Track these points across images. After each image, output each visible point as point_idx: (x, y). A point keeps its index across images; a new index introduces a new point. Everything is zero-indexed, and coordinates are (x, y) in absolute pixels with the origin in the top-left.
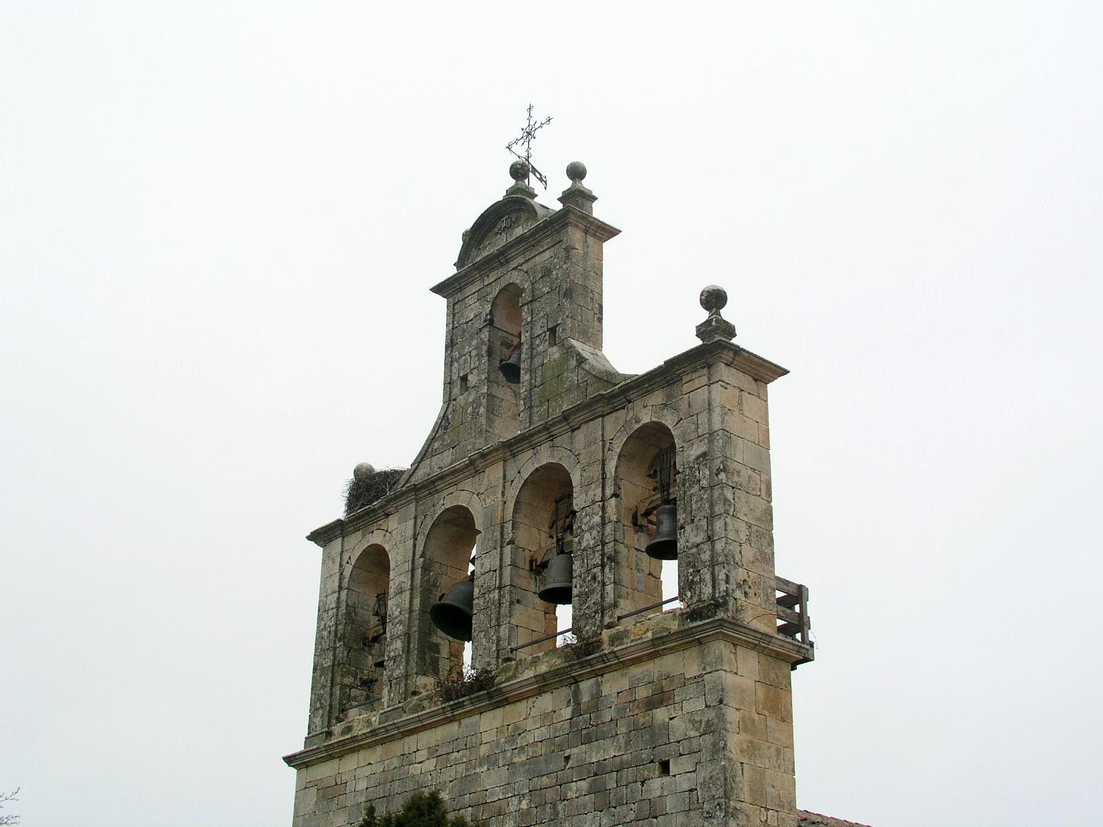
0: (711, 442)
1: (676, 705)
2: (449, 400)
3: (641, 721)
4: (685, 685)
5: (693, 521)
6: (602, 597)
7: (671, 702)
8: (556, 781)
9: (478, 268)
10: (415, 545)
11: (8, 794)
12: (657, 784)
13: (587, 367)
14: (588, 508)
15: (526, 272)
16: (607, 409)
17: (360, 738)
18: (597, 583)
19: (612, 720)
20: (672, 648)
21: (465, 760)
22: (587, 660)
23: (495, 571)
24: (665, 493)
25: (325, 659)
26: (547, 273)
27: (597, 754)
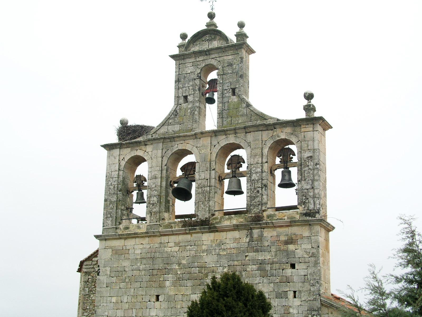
0: (314, 152)
1: (299, 245)
2: (178, 104)
3: (282, 248)
4: (302, 239)
5: (305, 180)
7: (296, 243)
8: (241, 263)
9: (195, 53)
11: (357, 297)
12: (289, 271)
13: (252, 109)
14: (254, 165)
16: (264, 129)
17: (139, 234)
19: (268, 246)
20: (297, 225)
21: (195, 250)
22: (260, 223)
24: (286, 164)
25: (112, 198)
26: (230, 65)
27: (261, 257)
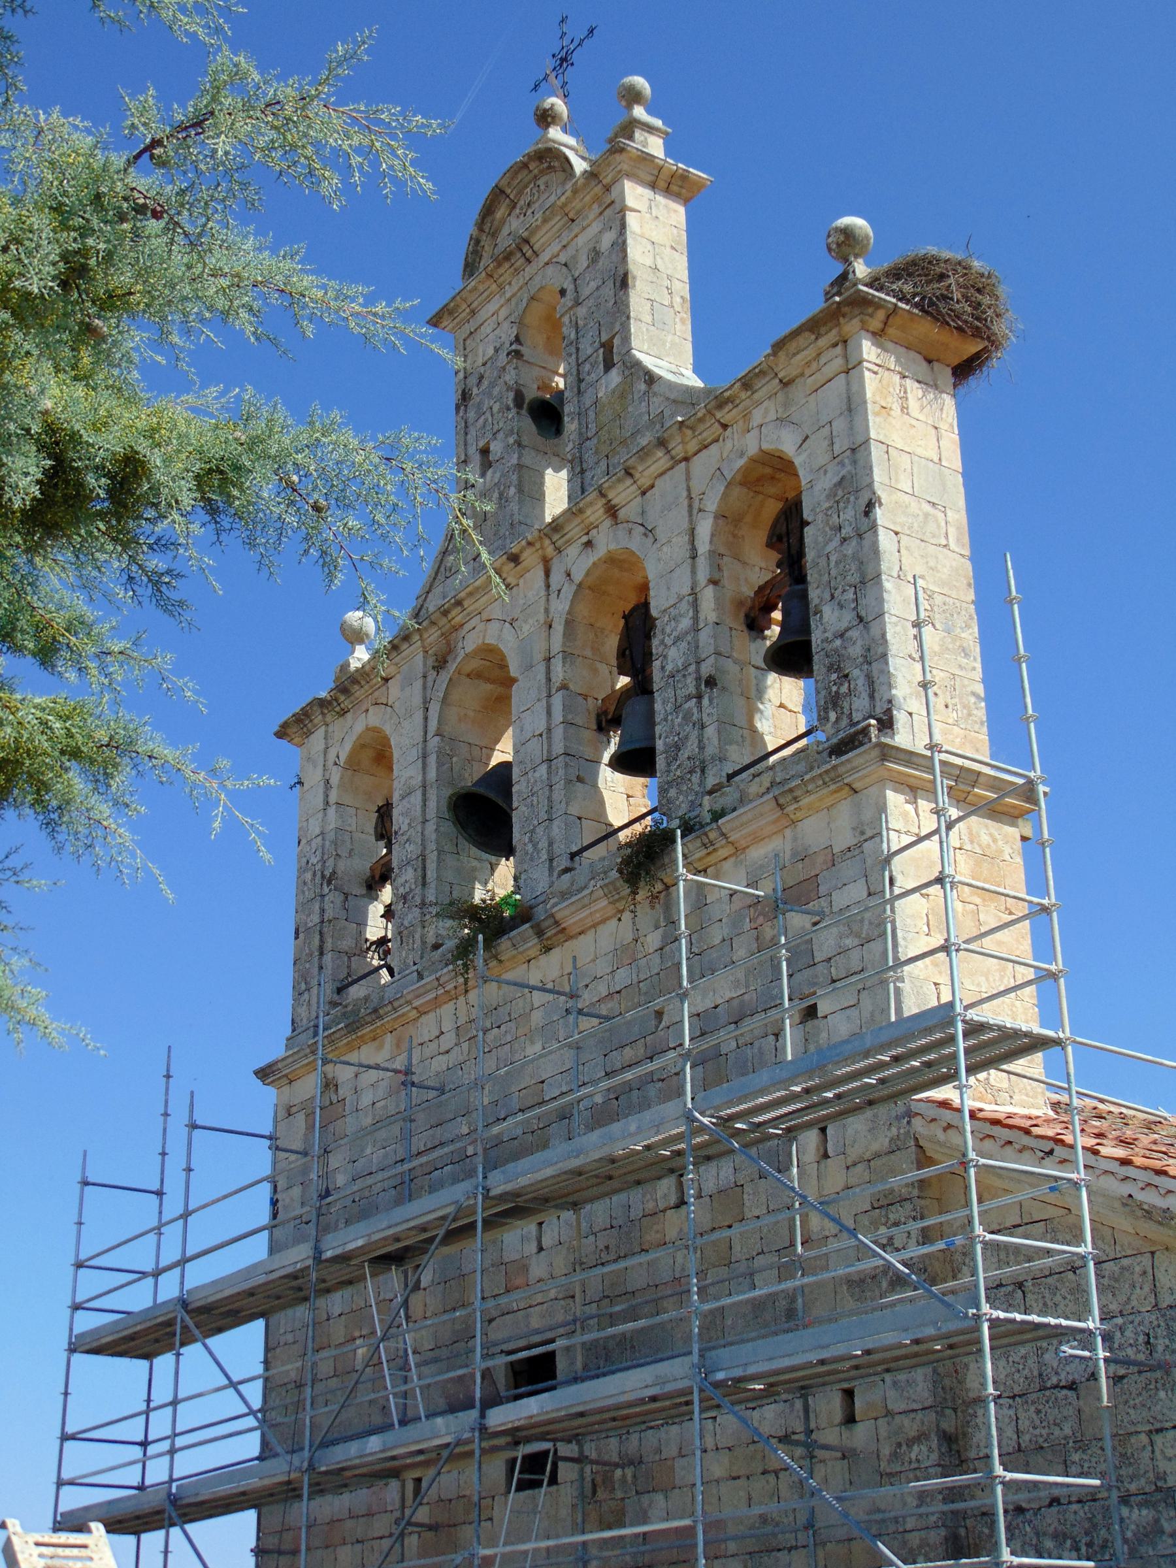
6: (702, 748)
10: (426, 719)
15: (565, 265)
18: (90, 242)
23: (541, 735)
